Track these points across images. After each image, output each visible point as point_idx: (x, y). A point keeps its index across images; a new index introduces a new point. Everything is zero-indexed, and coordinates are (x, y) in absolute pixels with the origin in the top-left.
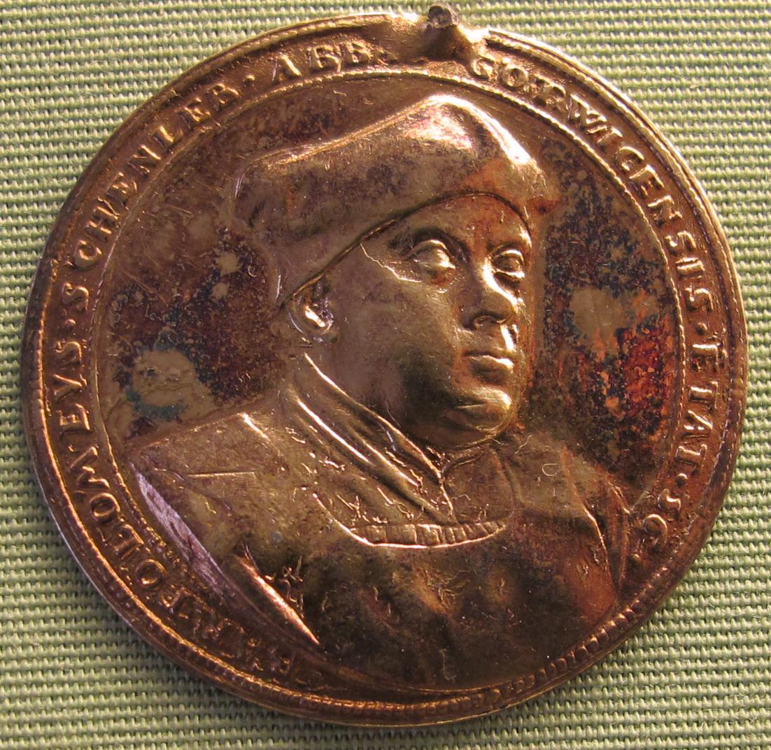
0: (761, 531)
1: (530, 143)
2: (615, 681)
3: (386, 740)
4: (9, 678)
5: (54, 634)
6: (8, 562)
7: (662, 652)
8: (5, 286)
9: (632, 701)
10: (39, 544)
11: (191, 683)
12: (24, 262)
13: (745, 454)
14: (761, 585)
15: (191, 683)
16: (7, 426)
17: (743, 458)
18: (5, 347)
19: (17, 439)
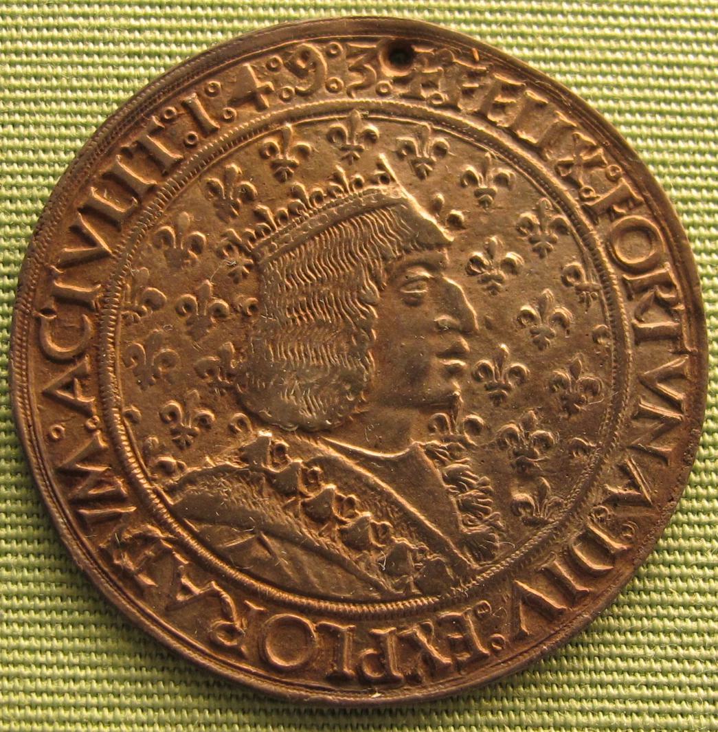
14: (707, 219)
18: (6, 263)
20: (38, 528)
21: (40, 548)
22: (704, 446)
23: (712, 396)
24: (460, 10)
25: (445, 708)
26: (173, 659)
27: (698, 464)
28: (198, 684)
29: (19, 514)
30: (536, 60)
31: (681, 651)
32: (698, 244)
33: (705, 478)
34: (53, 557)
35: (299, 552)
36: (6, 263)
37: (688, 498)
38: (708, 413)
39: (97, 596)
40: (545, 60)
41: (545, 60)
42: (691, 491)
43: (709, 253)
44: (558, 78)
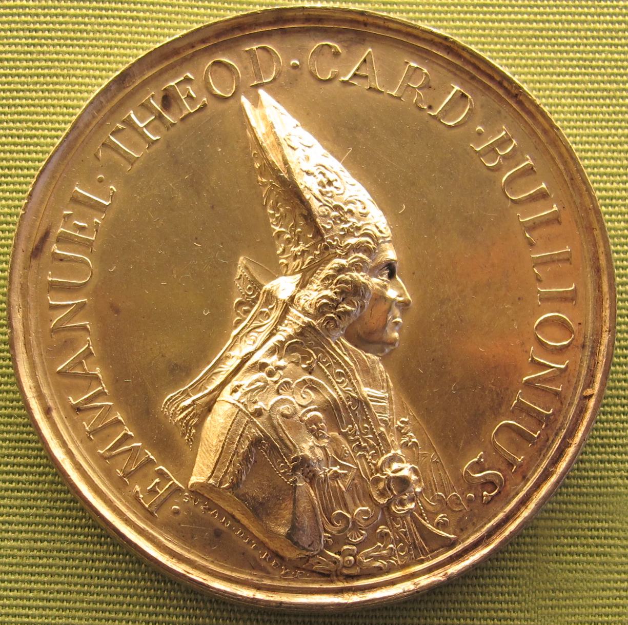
0: (623, 406)
4: (5, 124)
14: (622, 71)
24: (506, 6)
30: (461, 36)
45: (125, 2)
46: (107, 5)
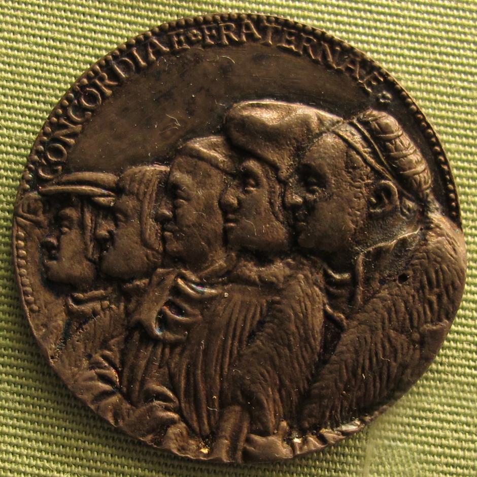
1: (278, 129)
2: (356, 452)
3: (157, 465)
4: (6, 35)
5: (18, 411)
6: (5, 155)
7: (20, 441)
8: (4, 103)
9: (68, 448)
10: (18, 341)
11: (95, 429)
12: (13, 171)
13: (466, 301)
15: (95, 429)
16: (2, 247)
17: (464, 303)
18: (3, 210)
19: (10, 292)
20: (15, 324)
21: (17, 345)
22: (449, 341)
23: (458, 318)
25: (242, 472)
26: (85, 410)
27: (437, 358)
28: (99, 436)
29: (13, 349)
31: (457, 378)
32: (465, 205)
33: (440, 368)
34: (17, 325)
35: (155, 252)
36: (3, 210)
37: (432, 371)
38: (464, 296)
39: (46, 371)
40: (362, 42)
41: (362, 42)
42: (450, 336)
43: (471, 212)
44: (369, 55)
45: (315, 2)
46: (304, 5)
